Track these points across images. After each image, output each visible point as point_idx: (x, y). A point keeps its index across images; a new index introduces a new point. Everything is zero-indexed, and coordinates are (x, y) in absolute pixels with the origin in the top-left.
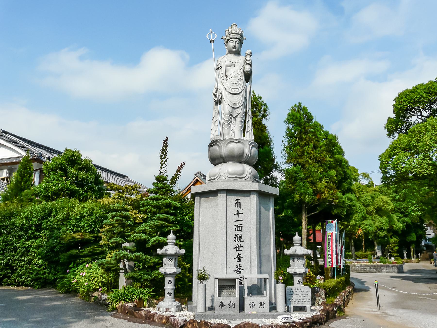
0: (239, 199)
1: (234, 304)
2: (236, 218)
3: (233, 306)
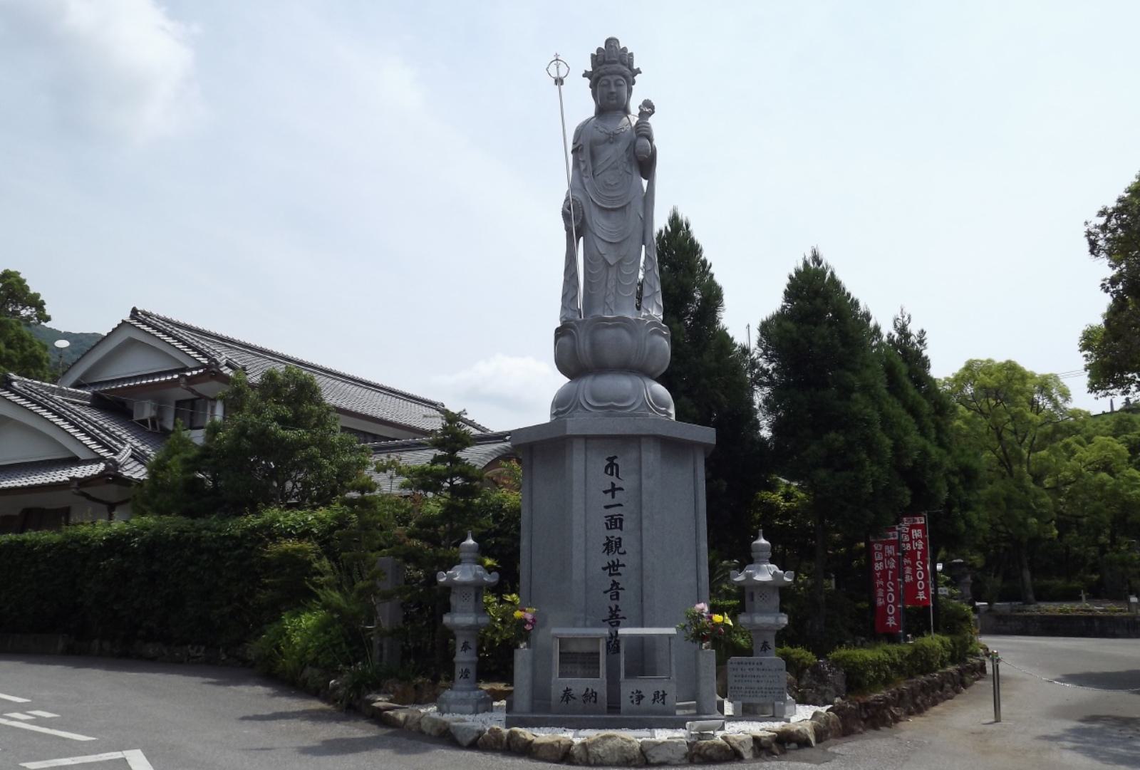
0: (615, 457)
1: (595, 694)
2: (608, 499)
3: (593, 699)
